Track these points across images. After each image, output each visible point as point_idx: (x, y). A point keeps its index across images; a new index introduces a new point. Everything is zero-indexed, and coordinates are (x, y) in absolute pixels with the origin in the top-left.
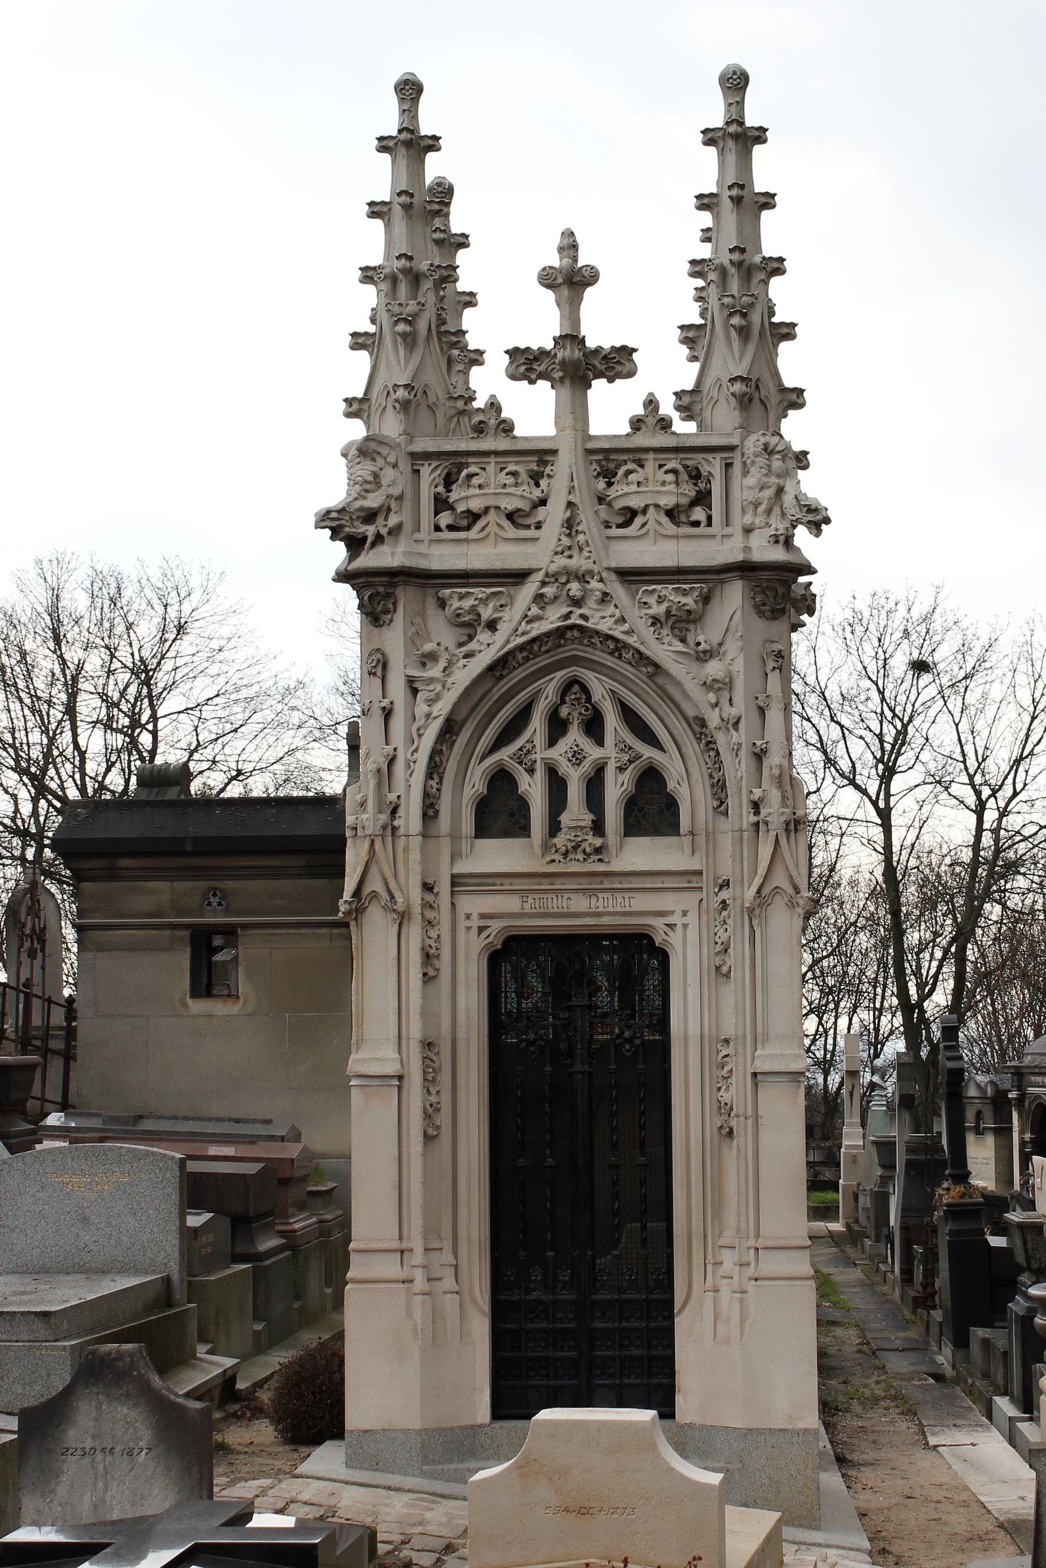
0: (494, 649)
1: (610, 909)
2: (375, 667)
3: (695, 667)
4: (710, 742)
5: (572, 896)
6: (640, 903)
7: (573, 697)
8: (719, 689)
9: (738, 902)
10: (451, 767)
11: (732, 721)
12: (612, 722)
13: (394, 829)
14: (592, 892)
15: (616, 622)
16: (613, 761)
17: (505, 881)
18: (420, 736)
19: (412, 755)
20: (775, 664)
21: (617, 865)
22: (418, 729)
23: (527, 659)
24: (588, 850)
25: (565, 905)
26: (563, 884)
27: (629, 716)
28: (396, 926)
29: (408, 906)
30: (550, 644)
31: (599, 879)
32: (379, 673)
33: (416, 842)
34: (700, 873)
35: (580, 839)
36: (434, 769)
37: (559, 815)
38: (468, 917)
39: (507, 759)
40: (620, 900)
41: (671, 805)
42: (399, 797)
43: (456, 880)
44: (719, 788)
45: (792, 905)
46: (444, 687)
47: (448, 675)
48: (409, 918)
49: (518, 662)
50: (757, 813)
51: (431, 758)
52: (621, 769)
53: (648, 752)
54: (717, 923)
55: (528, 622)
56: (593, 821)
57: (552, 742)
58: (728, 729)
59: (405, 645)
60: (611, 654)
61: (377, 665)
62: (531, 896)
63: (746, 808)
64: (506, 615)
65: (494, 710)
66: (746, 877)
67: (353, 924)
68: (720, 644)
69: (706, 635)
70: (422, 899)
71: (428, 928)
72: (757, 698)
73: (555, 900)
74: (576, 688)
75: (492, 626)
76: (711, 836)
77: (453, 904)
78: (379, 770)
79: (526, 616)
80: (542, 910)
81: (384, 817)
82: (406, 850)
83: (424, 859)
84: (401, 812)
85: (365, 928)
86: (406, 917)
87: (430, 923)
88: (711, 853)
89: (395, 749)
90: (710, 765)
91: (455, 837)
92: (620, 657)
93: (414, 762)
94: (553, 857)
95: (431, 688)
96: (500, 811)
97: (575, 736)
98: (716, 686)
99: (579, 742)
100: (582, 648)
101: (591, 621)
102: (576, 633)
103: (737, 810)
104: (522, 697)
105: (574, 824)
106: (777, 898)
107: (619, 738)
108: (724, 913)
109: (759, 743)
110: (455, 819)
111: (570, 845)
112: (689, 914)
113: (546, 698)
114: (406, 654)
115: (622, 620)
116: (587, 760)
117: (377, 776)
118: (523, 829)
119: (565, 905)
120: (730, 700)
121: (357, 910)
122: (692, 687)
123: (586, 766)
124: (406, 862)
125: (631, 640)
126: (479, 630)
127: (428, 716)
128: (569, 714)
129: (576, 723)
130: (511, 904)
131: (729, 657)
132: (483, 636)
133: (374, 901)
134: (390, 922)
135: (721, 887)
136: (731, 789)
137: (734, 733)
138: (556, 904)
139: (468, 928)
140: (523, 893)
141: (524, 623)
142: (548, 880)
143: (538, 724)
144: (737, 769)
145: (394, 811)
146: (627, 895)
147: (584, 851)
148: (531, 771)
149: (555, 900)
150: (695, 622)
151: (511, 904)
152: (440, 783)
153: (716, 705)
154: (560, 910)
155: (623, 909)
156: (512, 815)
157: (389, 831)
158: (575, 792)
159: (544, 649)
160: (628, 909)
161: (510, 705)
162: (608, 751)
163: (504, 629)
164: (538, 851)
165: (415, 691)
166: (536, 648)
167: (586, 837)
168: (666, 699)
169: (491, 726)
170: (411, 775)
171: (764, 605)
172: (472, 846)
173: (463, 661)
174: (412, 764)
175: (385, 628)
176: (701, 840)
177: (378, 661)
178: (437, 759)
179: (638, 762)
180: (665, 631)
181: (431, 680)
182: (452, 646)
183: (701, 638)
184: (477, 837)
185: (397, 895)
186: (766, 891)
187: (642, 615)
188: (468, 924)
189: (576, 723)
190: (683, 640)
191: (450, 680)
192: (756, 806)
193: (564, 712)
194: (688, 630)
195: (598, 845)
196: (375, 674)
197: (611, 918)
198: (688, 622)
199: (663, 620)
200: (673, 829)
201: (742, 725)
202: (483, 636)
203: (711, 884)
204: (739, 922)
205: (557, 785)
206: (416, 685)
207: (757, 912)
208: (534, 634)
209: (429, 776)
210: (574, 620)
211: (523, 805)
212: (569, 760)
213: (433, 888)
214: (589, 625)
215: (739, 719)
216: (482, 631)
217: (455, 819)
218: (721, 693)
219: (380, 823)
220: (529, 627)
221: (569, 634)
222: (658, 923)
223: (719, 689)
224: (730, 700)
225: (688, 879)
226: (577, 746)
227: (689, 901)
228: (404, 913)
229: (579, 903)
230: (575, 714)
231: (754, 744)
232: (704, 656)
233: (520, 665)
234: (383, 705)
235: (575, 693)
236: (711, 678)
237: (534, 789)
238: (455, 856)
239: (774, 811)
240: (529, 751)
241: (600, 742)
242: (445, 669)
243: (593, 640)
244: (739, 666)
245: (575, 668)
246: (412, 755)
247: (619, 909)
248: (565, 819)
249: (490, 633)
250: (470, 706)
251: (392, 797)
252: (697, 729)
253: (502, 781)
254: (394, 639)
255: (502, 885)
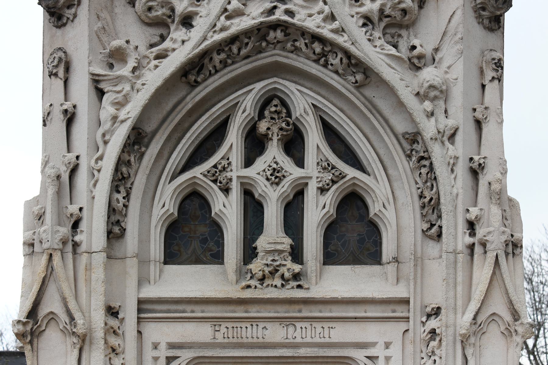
0: (189, 46)
1: (309, 340)
2: (57, 66)
3: (408, 75)
4: (422, 158)
5: (268, 325)
6: (341, 333)
7: (273, 109)
8: (436, 98)
9: (451, 331)
10: (139, 182)
11: (448, 133)
12: (314, 139)
13: (76, 245)
14: (287, 321)
15: (325, 20)
16: (314, 180)
17: (197, 308)
18: (106, 143)
19: (96, 162)
20: (494, 74)
21: (316, 291)
22: (104, 135)
23: (224, 64)
24: (287, 275)
25: (260, 335)
26: (258, 312)
27: (330, 133)
28: (76, 352)
29: (90, 330)
30: (250, 46)
31: (297, 307)
32: (61, 73)
33: (99, 259)
34: (406, 302)
35: (278, 263)
36: (121, 180)
37: (254, 241)
38: (156, 346)
39: (201, 177)
40: (319, 330)
41: (373, 231)
42: (81, 209)
43: (142, 305)
44: (431, 207)
45: (508, 333)
46: (132, 88)
47: (138, 77)
48: (91, 343)
49: (215, 67)
50: (473, 234)
51: (117, 169)
52: (322, 190)
53: (351, 172)
54: (423, 355)
55: (228, 18)
56: (291, 245)
57: (248, 162)
58: (443, 143)
59: (90, 40)
60: (317, 61)
61: (59, 67)
62: (224, 325)
63: (462, 226)
64: (202, 10)
65: (186, 125)
66: (460, 303)
67: (28, 354)
68: (436, 50)
69: (424, 39)
70: (106, 324)
71: (112, 355)
72: (475, 110)
73: (249, 329)
74: (276, 102)
75: (187, 21)
76: (419, 261)
77: (139, 332)
78: (58, 177)
79: (226, 10)
80: (235, 340)
81: (65, 230)
82: (89, 268)
83: (108, 281)
84: (83, 226)
85: (41, 353)
86: (88, 338)
87: (114, 350)
88: (419, 281)
89: (78, 157)
90: (421, 185)
91: (143, 261)
92: (325, 66)
93: (99, 171)
94: (248, 283)
95: (118, 88)
96: (191, 234)
97: (274, 153)
98: (432, 94)
99: (278, 160)
100: (285, 54)
101: (297, 17)
102: (279, 34)
103: (452, 230)
104: (217, 110)
105: (272, 247)
106: (493, 326)
107: (321, 157)
108: (433, 344)
109: (476, 158)
110: (144, 240)
111: (267, 270)
112: (391, 346)
113: (244, 111)
114: (91, 50)
115: (332, 17)
116: (285, 180)
117: (56, 182)
118: (217, 257)
119: (260, 335)
120: (446, 112)
121: (32, 333)
122: (407, 96)
123: (286, 186)
124: (88, 281)
125: (340, 40)
126: (173, 27)
127: (115, 118)
128: (268, 129)
129: (275, 138)
130: (202, 333)
131: (445, 64)
132: (178, 33)
133: (53, 323)
134: (69, 347)
135: (429, 316)
136: (445, 207)
137: (450, 146)
138: (249, 333)
139: (156, 359)
140: (216, 320)
141: (223, 18)
142: (242, 308)
143: (234, 138)
144: (453, 186)
145: (76, 225)
146: (326, 325)
147: (282, 277)
148: (226, 190)
149: (249, 329)
150: (407, 27)
151: (202, 333)
152: (127, 197)
153: (432, 114)
154: (255, 340)
155: (322, 340)
156: (204, 241)
157: (69, 247)
158: (273, 215)
159: (244, 52)
160: (327, 340)
161: (204, 118)
162: (309, 171)
163: (201, 25)
164: (232, 276)
165: (101, 93)
166: (235, 49)
167: (284, 262)
168: (374, 112)
169: (184, 141)
170: (95, 185)
171: (484, 9)
172: (161, 271)
173: (156, 62)
174: (96, 173)
175: (68, 27)
176: (408, 268)
177: (60, 60)
178: (124, 170)
179: (341, 182)
180: (377, 34)
181: (119, 79)
182: (142, 49)
183: (416, 42)
184: (165, 263)
185: (77, 315)
186: (480, 319)
187: (353, 13)
188: (156, 353)
189: (275, 138)
190: (395, 46)
191: (139, 82)
192: (471, 226)
193: (263, 127)
194: (400, 36)
195: (297, 271)
196: (56, 75)
197: (309, 350)
198: (400, 26)
199: (376, 19)
200: (375, 257)
201: (459, 138)
202: (178, 33)
203: (418, 313)
204: (451, 351)
205: (253, 208)
206: (102, 86)
207: (472, 340)
208: (233, 30)
209: (115, 188)
210: (279, 15)
211: (217, 230)
212: (268, 179)
213: (117, 313)
214: (295, 21)
215: (456, 130)
216: (176, 29)
217: (144, 240)
218: (436, 103)
219: (59, 236)
220: (228, 23)
221: (272, 34)
222: (359, 355)
223: (436, 98)
224: (446, 112)
225: (395, 307)
226: (276, 163)
227: (393, 331)
228: (85, 336)
229: (275, 333)
230: (275, 129)
231: (471, 159)
232: (416, 63)
233: (217, 71)
234: (65, 107)
235: (276, 106)
236: (426, 85)
237: (228, 210)
238: (142, 281)
239: (492, 230)
240: (224, 169)
241: (300, 163)
242: (134, 69)
243: (297, 44)
244: (458, 71)
245: (275, 79)
246: (96, 162)
247: (317, 340)
248: (262, 243)
249: (184, 30)
250: (161, 116)
251: (73, 209)
252: (407, 146)
253: (193, 203)
254: (78, 37)
255: (193, 312)
